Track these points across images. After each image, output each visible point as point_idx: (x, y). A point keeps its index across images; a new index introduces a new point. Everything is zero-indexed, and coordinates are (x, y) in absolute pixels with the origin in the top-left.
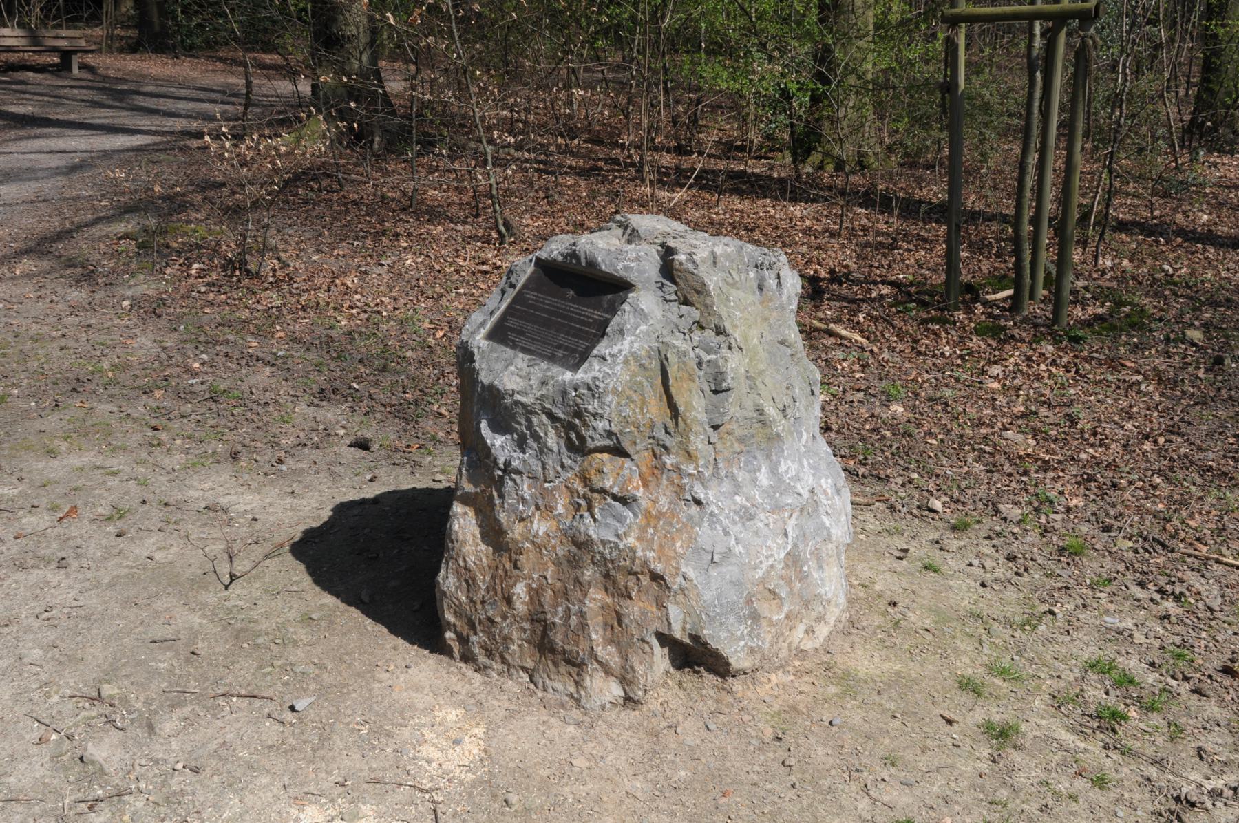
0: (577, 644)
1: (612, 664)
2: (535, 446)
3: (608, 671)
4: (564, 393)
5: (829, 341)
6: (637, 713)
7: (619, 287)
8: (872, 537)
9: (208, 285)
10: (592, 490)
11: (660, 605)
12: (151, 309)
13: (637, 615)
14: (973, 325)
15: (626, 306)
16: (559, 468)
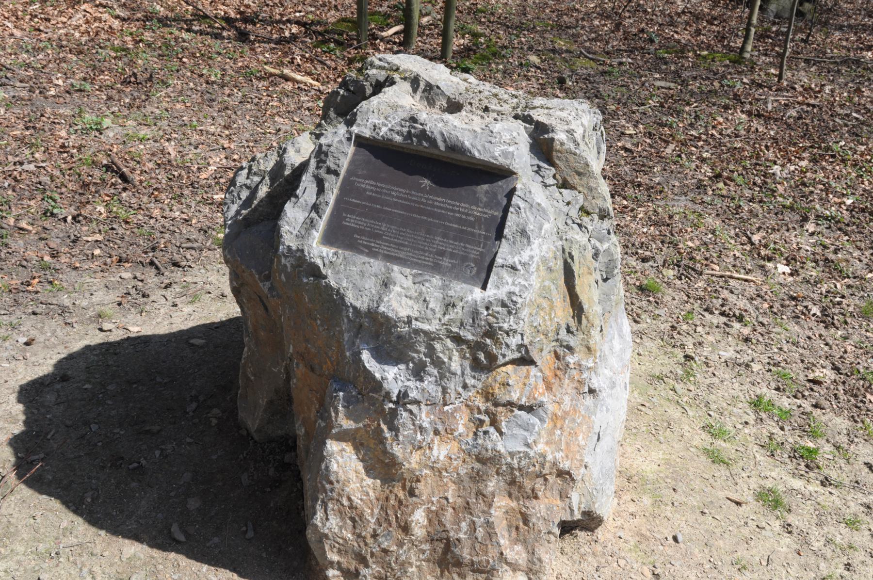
0: (486, 553)
1: (520, 562)
2: (435, 372)
4: (475, 314)
7: (497, 173)
10: (496, 405)
11: (563, 495)
16: (460, 390)
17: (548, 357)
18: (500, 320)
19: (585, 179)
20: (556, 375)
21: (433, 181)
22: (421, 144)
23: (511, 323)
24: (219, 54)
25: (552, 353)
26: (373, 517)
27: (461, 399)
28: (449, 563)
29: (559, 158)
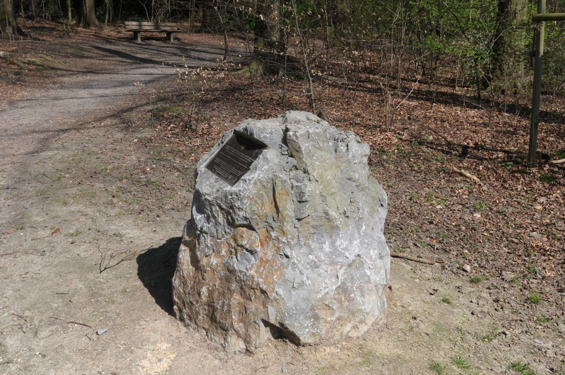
1: (241, 332)
3: (239, 336)
4: (226, 197)
5: (459, 179)
6: (251, 358)
8: (423, 281)
9: (173, 134)
10: (238, 245)
12: (145, 143)
14: (539, 175)
15: (261, 156)
16: (224, 233)
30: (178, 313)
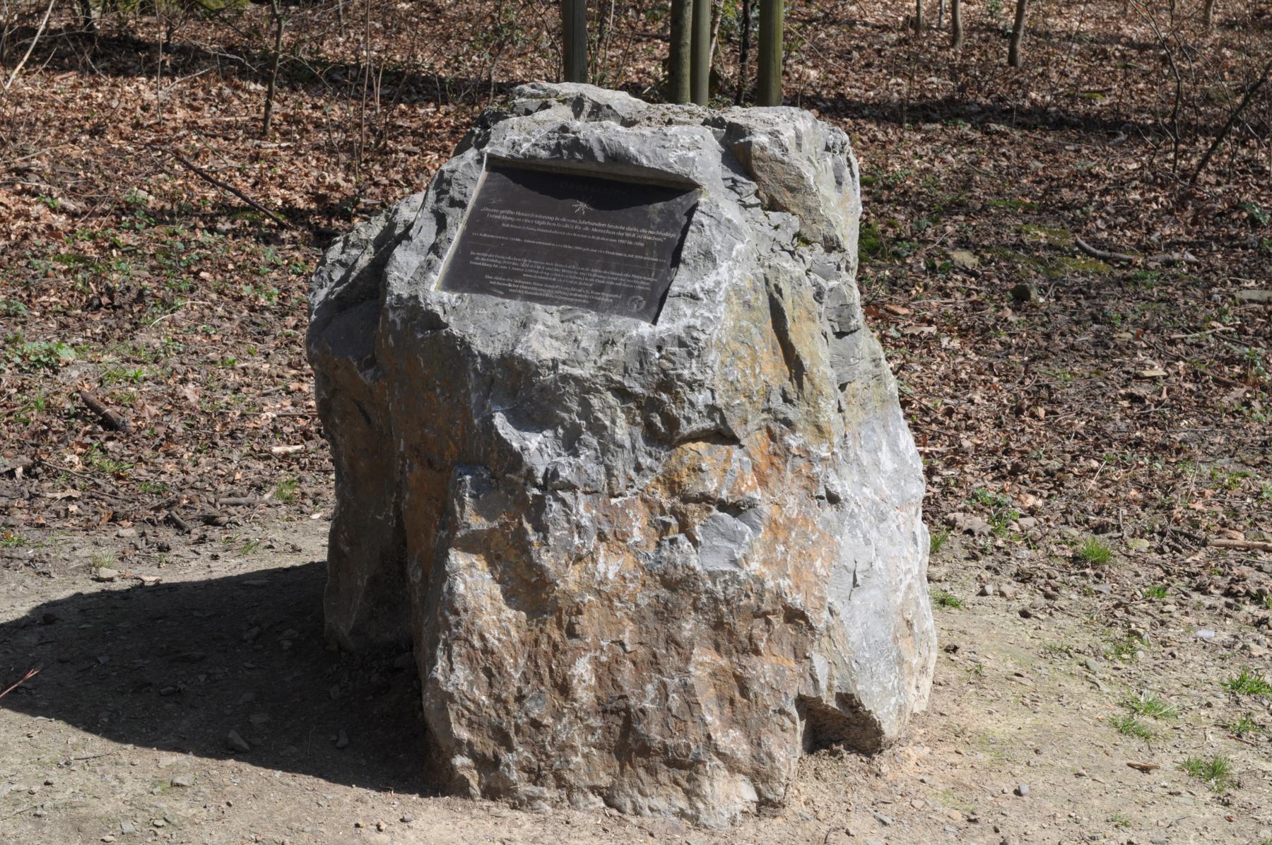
0: (686, 736)
1: (739, 755)
2: (595, 442)
3: (732, 766)
4: (643, 355)
6: (779, 820)
7: (676, 188)
10: (686, 499)
13: (770, 676)
16: (632, 473)
17: (759, 436)
18: (678, 366)
19: (799, 196)
20: (772, 464)
21: (589, 203)
22: (573, 158)
23: (694, 370)
24: (274, 266)
25: (764, 430)
26: (516, 671)
27: (635, 490)
28: (632, 750)
29: (760, 168)
30: (473, 778)
